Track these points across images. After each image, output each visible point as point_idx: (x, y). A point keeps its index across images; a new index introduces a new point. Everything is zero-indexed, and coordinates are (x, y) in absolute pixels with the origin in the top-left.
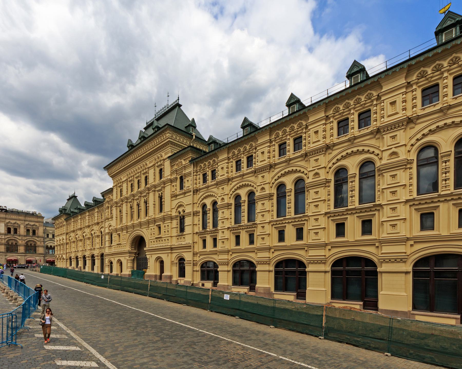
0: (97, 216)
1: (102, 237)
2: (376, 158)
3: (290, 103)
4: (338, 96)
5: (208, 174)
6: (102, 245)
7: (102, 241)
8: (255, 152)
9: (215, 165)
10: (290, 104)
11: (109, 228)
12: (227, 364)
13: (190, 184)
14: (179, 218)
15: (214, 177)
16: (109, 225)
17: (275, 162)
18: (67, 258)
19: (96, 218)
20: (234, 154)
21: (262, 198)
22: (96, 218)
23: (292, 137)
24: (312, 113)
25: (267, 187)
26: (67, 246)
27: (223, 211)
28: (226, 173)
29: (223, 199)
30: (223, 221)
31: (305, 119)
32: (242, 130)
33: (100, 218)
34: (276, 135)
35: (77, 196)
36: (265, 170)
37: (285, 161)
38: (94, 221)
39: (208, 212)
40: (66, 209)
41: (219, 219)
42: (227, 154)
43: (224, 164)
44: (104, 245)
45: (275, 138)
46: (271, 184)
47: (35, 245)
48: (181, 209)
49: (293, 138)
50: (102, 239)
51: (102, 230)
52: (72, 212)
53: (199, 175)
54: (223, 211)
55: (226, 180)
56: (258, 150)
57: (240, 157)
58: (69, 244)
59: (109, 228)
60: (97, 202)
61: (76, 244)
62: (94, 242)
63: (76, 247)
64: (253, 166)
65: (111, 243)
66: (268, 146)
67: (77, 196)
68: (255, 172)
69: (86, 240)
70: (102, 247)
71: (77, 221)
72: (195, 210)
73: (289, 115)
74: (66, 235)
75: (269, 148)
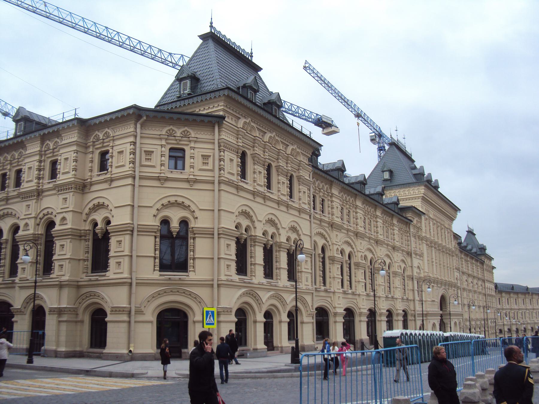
2: (49, 216)
3: (181, 77)
4: (119, 115)
5: (9, 175)
8: (113, 146)
9: (109, 142)
10: (181, 78)
13: (33, 176)
15: (18, 183)
17: (91, 179)
20: (49, 148)
21: (63, 235)
23: (48, 158)
24: (35, 142)
25: (69, 217)
27: (229, 243)
28: (35, 178)
29: (64, 219)
31: (112, 127)
32: (14, 123)
34: (106, 135)
36: (61, 190)
37: (105, 181)
39: (3, 246)
41: (55, 257)
42: (39, 145)
43: (33, 163)
45: (45, 151)
46: (38, 220)
47: (184, 223)
48: (99, 217)
49: (100, 152)
53: (93, 152)
54: (119, 238)
55: (108, 180)
56: (61, 154)
57: (108, 146)
60: (28, 124)
64: (107, 170)
66: (74, 151)
68: (19, 196)
73: (16, 136)
75: (75, 154)
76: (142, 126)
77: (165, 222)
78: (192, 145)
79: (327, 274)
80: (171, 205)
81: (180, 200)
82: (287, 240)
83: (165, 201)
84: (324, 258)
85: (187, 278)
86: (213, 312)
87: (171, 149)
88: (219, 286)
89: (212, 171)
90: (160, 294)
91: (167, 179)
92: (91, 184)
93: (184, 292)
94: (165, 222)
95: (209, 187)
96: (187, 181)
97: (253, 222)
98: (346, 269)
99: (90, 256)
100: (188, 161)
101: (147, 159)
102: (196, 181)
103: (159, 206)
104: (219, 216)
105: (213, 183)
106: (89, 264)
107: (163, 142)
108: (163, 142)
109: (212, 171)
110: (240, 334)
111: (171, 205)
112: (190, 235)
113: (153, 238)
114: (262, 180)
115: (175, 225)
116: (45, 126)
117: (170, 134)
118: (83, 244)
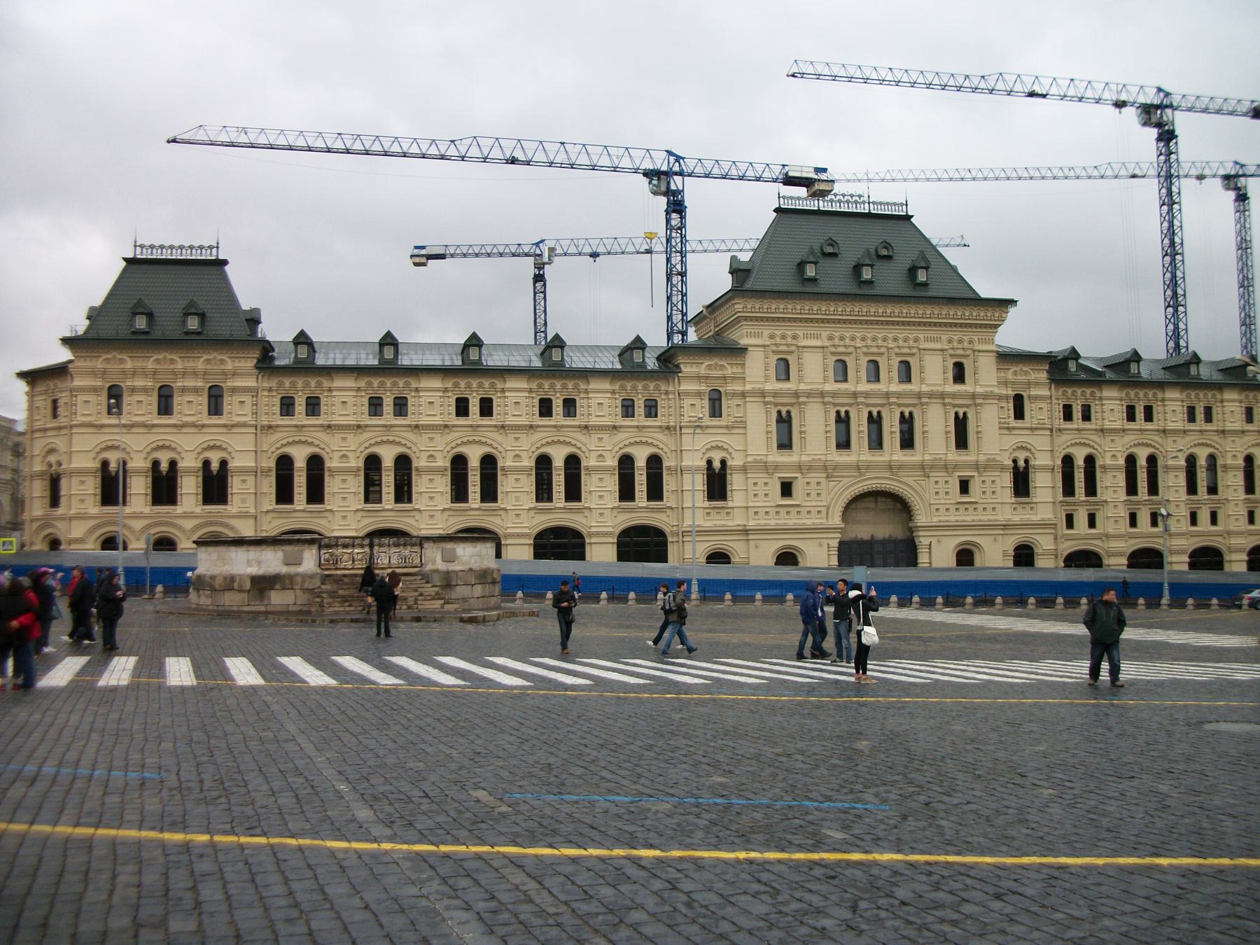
11: (45, 456)
47: (173, 464)
59: (45, 456)
77: (156, 464)
93: (222, 524)
96: (225, 426)
102: (183, 426)
111: (1022, 448)
115: (164, 466)
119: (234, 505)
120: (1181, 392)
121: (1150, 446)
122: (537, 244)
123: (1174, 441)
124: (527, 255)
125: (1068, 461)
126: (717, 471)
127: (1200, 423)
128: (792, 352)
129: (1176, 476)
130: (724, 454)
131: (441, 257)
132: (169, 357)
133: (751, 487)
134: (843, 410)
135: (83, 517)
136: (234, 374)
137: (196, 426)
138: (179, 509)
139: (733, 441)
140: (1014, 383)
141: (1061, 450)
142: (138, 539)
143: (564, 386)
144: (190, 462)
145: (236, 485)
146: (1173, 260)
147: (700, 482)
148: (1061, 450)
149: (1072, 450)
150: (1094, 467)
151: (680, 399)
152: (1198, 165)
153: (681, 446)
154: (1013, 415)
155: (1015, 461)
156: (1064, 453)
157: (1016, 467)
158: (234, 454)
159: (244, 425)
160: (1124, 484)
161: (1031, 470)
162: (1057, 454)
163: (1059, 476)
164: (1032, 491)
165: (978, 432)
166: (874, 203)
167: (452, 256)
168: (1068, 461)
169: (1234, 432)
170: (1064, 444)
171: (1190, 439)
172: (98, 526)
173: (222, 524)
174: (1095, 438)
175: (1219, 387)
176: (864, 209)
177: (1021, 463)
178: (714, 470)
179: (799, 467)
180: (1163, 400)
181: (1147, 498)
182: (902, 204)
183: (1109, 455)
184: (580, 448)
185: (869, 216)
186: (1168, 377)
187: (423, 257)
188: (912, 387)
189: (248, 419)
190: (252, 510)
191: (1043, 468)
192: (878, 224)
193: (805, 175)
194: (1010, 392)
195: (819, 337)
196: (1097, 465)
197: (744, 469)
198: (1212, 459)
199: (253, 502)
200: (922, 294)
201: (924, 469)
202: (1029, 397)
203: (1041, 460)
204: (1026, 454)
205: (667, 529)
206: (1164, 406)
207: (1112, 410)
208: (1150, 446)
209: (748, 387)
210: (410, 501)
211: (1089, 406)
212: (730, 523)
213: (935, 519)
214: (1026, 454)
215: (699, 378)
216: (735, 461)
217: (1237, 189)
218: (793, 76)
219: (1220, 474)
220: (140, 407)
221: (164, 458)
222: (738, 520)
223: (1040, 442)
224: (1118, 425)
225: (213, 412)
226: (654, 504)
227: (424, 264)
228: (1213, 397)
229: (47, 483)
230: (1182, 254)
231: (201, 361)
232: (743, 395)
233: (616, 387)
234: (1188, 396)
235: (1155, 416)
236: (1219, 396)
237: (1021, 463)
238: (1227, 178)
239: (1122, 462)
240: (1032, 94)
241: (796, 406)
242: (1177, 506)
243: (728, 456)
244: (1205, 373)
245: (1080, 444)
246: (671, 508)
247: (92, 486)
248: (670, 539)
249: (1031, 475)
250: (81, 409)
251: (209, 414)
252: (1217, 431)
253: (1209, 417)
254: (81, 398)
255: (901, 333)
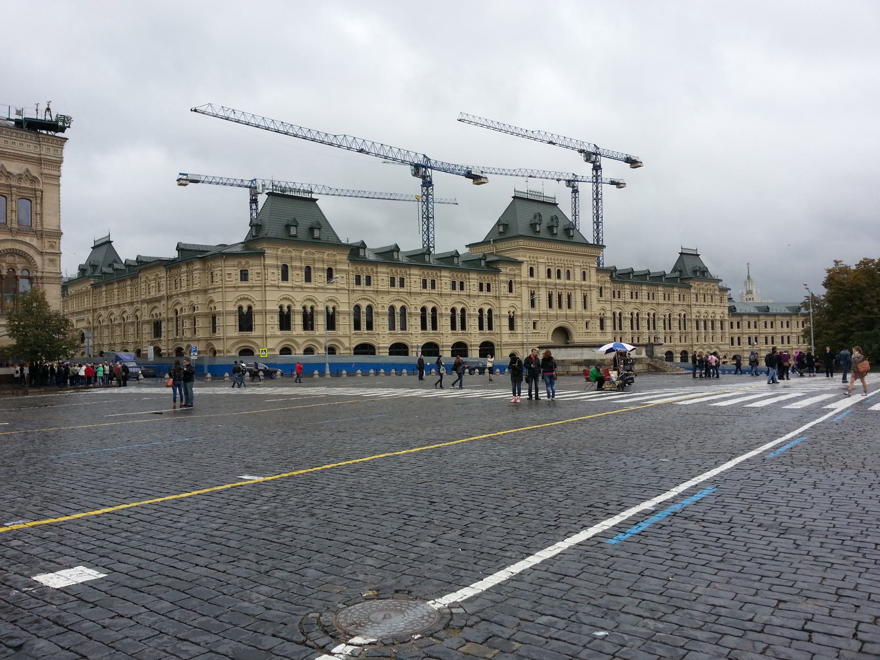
0: (186, 279)
1: (177, 321)
6: (177, 334)
7: (177, 328)
11: (209, 305)
12: (417, 601)
14: (153, 323)
16: (210, 299)
18: (170, 351)
19: (129, 295)
21: (184, 317)
22: (184, 283)
26: (96, 332)
27: (344, 317)
30: (272, 326)
33: (174, 288)
35: (317, 200)
38: (193, 284)
40: (97, 266)
42: (165, 273)
44: (181, 334)
47: (250, 308)
50: (177, 324)
51: (138, 314)
52: (105, 273)
54: (344, 317)
58: (99, 328)
59: (209, 305)
61: (122, 328)
62: (141, 329)
63: (123, 335)
65: (214, 331)
67: (317, 200)
69: (127, 325)
70: (178, 337)
71: (101, 293)
72: (169, 316)
73: (78, 278)
74: (93, 313)
76: (224, 260)
77: (240, 308)
78: (251, 268)
79: (640, 325)
80: (286, 299)
81: (246, 297)
82: (509, 313)
83: (239, 298)
84: (685, 320)
85: (251, 335)
86: (265, 351)
87: (241, 271)
88: (266, 338)
89: (262, 280)
90: (237, 343)
91: (239, 287)
92: (208, 290)
93: (250, 342)
94: (240, 308)
95: (259, 289)
96: (249, 287)
97: (516, 309)
98: (682, 322)
99: (237, 323)
100: (250, 277)
101: (229, 277)
102: (319, 288)
103: (236, 300)
104: (265, 303)
105: (225, 287)
106: (326, 326)
107: (236, 268)
108: (236, 268)
109: (262, 280)
110: (124, 374)
111: (286, 299)
112: (315, 314)
113: (234, 317)
114: (702, 300)
115: (245, 309)
116: (147, 263)
117: (240, 263)
118: (208, 319)
119: (257, 332)
120: (450, 273)
121: (403, 301)
122: (252, 181)
123: (415, 299)
124: (247, 187)
125: (357, 308)
126: (285, 313)
127: (429, 289)
128: (535, 264)
129: (416, 319)
130: (249, 303)
131: (197, 182)
132: (312, 251)
133: (524, 324)
134: (551, 291)
135: (274, 337)
136: (340, 262)
137: (323, 289)
138: (254, 333)
139: (517, 303)
140: (306, 260)
141: (354, 302)
142: (299, 349)
143: (367, 269)
144: (321, 308)
145: (257, 320)
146: (427, 197)
147: (276, 320)
148: (354, 302)
149: (482, 306)
150: (492, 315)
151: (265, 269)
152: (558, 174)
153: (265, 298)
154: (304, 280)
155: (304, 308)
156: (355, 304)
157: (328, 312)
158: (340, 304)
159: (344, 289)
160: (420, 324)
161: (336, 314)
162: (351, 305)
163: (352, 318)
164: (292, 327)
165: (576, 301)
166: (545, 197)
167: (203, 182)
168: (357, 308)
169: (417, 294)
170: (355, 298)
171: (423, 298)
172: (237, 343)
173: (250, 342)
174: (373, 295)
175: (409, 266)
176: (541, 199)
177: (285, 309)
178: (283, 312)
179: (539, 316)
180: (377, 273)
181: (366, 332)
182: (552, 198)
183: (380, 306)
184: (406, 303)
185: (543, 202)
186: (380, 259)
187: (184, 180)
188: (587, 283)
189: (345, 286)
190: (348, 333)
191: (344, 313)
192: (535, 204)
193: (477, 174)
194: (280, 263)
195: (543, 258)
196: (407, 313)
197: (522, 316)
198: (403, 309)
199: (348, 329)
200: (555, 238)
201: (576, 317)
202: (292, 266)
203: (343, 308)
204: (334, 304)
205: (495, 343)
206: (377, 276)
207: (383, 279)
208: (403, 301)
209: (523, 279)
210: (312, 329)
211: (370, 277)
212: (517, 340)
213: (579, 339)
214: (334, 304)
215: (507, 274)
216: (519, 313)
217: (573, 187)
218: (460, 120)
219: (623, 321)
220: (297, 277)
221: (245, 305)
222: (519, 339)
223: (608, 307)
224: (385, 288)
225: (243, 279)
226: (369, 332)
227: (185, 185)
228: (371, 270)
229: (211, 319)
230: (432, 195)
231: (326, 254)
232: (521, 283)
233: (236, 263)
234: (391, 270)
235: (372, 282)
236: (375, 270)
237: (285, 309)
238: (569, 181)
239: (387, 310)
240: (550, 143)
241: (537, 289)
242: (475, 336)
243: (252, 304)
244: (403, 259)
245: (364, 299)
246: (497, 334)
247: (274, 320)
248: (496, 347)
249: (292, 317)
250: (270, 277)
251: (241, 280)
252: (373, 291)
253: (368, 282)
254: (270, 271)
255: (566, 257)
